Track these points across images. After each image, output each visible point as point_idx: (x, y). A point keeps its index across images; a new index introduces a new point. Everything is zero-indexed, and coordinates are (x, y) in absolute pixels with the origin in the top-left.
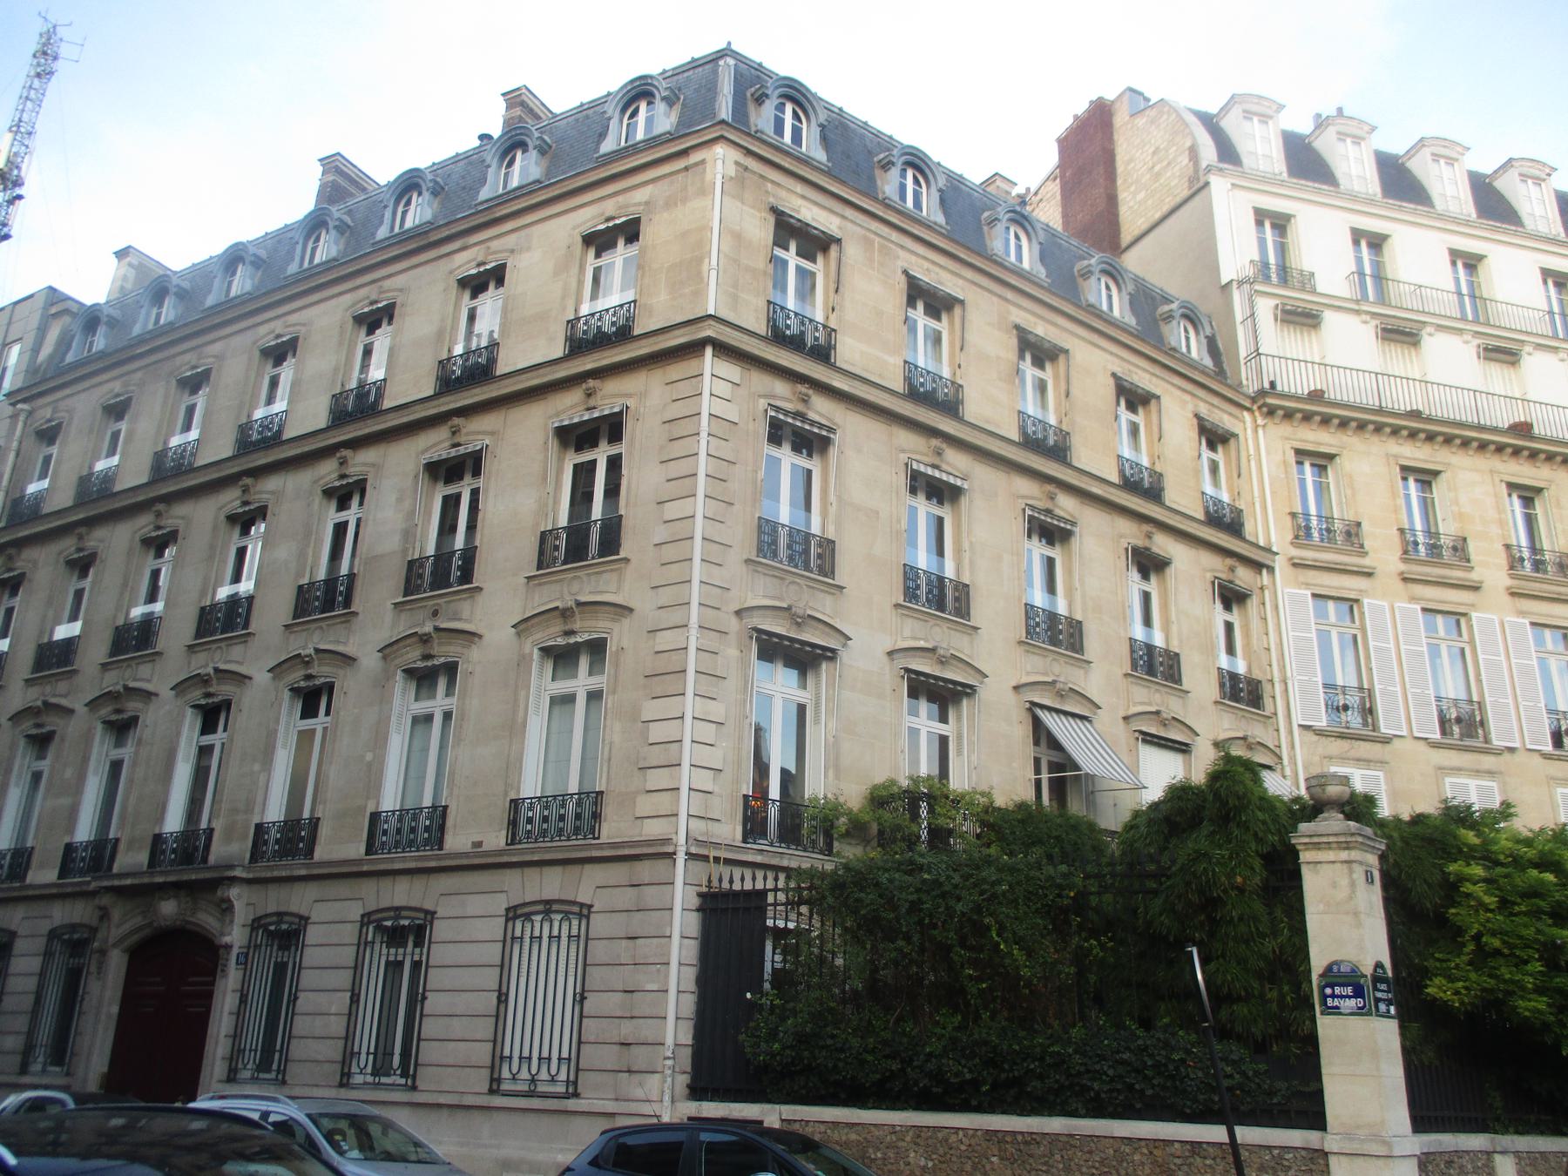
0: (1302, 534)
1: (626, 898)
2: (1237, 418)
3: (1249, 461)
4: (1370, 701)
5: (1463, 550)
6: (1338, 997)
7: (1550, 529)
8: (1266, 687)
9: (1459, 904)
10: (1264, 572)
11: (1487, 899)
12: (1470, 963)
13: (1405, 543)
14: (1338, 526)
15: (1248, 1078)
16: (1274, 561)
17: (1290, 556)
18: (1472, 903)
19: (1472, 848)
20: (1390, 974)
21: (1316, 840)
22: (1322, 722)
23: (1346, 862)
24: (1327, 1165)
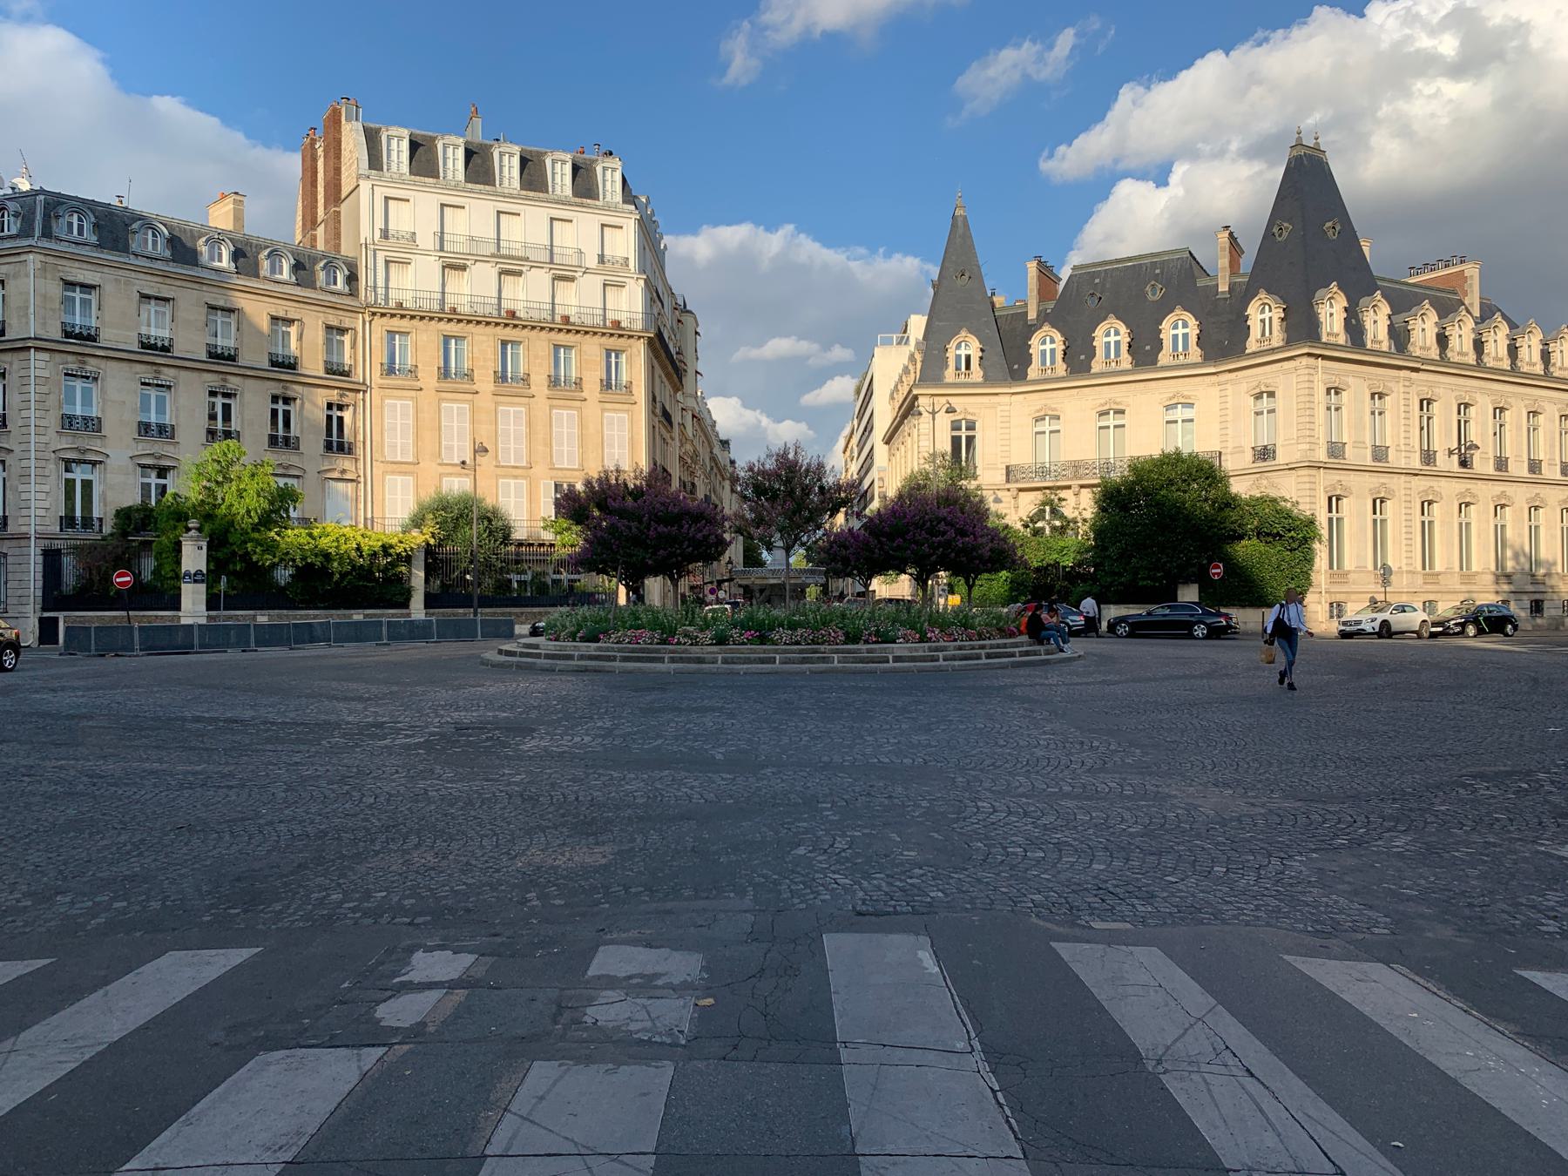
1: (17, 552)
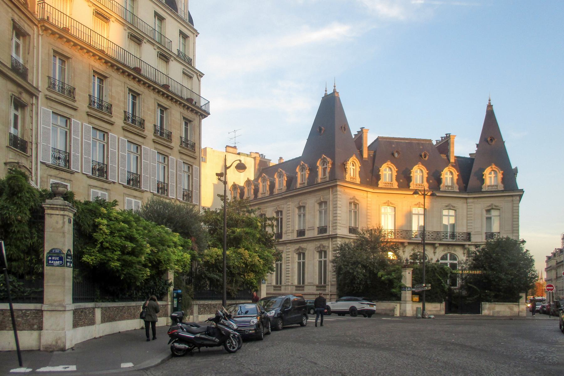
0: (51, 86)
2: (31, 27)
3: (34, 48)
4: (69, 157)
5: (110, 109)
6: (53, 260)
7: (139, 109)
8: (29, 145)
9: (97, 232)
10: (34, 98)
11: (106, 231)
12: (98, 251)
13: (90, 100)
14: (165, 131)
15: (15, 287)
16: (39, 94)
17: (87, 111)
18: (102, 232)
19: (104, 214)
20: (72, 254)
21: (52, 206)
22: (50, 161)
23: (62, 215)
24: (42, 315)
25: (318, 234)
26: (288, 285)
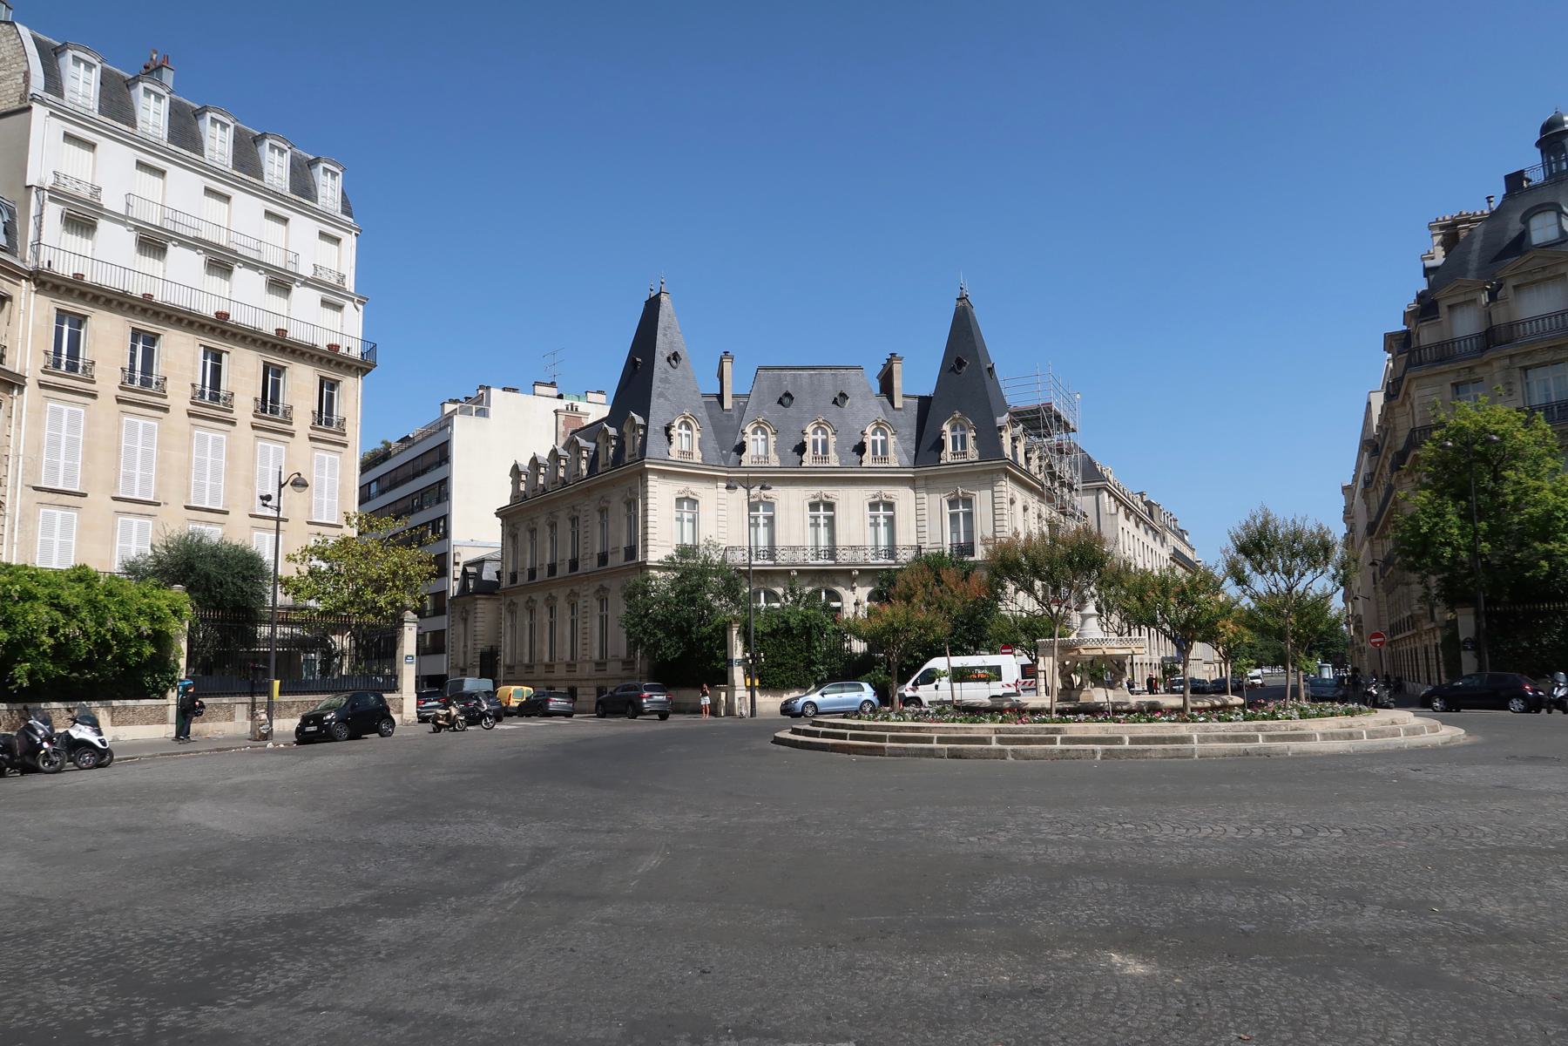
25: (626, 560)
26: (585, 661)
